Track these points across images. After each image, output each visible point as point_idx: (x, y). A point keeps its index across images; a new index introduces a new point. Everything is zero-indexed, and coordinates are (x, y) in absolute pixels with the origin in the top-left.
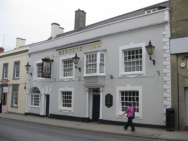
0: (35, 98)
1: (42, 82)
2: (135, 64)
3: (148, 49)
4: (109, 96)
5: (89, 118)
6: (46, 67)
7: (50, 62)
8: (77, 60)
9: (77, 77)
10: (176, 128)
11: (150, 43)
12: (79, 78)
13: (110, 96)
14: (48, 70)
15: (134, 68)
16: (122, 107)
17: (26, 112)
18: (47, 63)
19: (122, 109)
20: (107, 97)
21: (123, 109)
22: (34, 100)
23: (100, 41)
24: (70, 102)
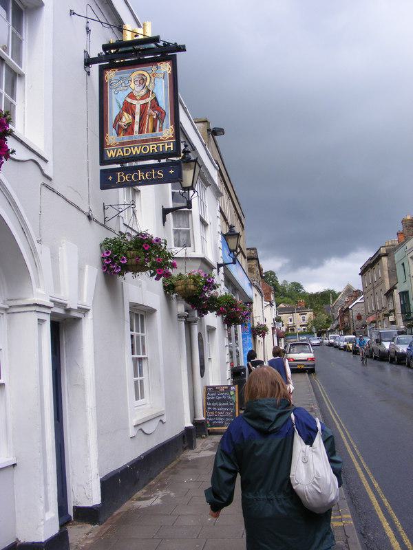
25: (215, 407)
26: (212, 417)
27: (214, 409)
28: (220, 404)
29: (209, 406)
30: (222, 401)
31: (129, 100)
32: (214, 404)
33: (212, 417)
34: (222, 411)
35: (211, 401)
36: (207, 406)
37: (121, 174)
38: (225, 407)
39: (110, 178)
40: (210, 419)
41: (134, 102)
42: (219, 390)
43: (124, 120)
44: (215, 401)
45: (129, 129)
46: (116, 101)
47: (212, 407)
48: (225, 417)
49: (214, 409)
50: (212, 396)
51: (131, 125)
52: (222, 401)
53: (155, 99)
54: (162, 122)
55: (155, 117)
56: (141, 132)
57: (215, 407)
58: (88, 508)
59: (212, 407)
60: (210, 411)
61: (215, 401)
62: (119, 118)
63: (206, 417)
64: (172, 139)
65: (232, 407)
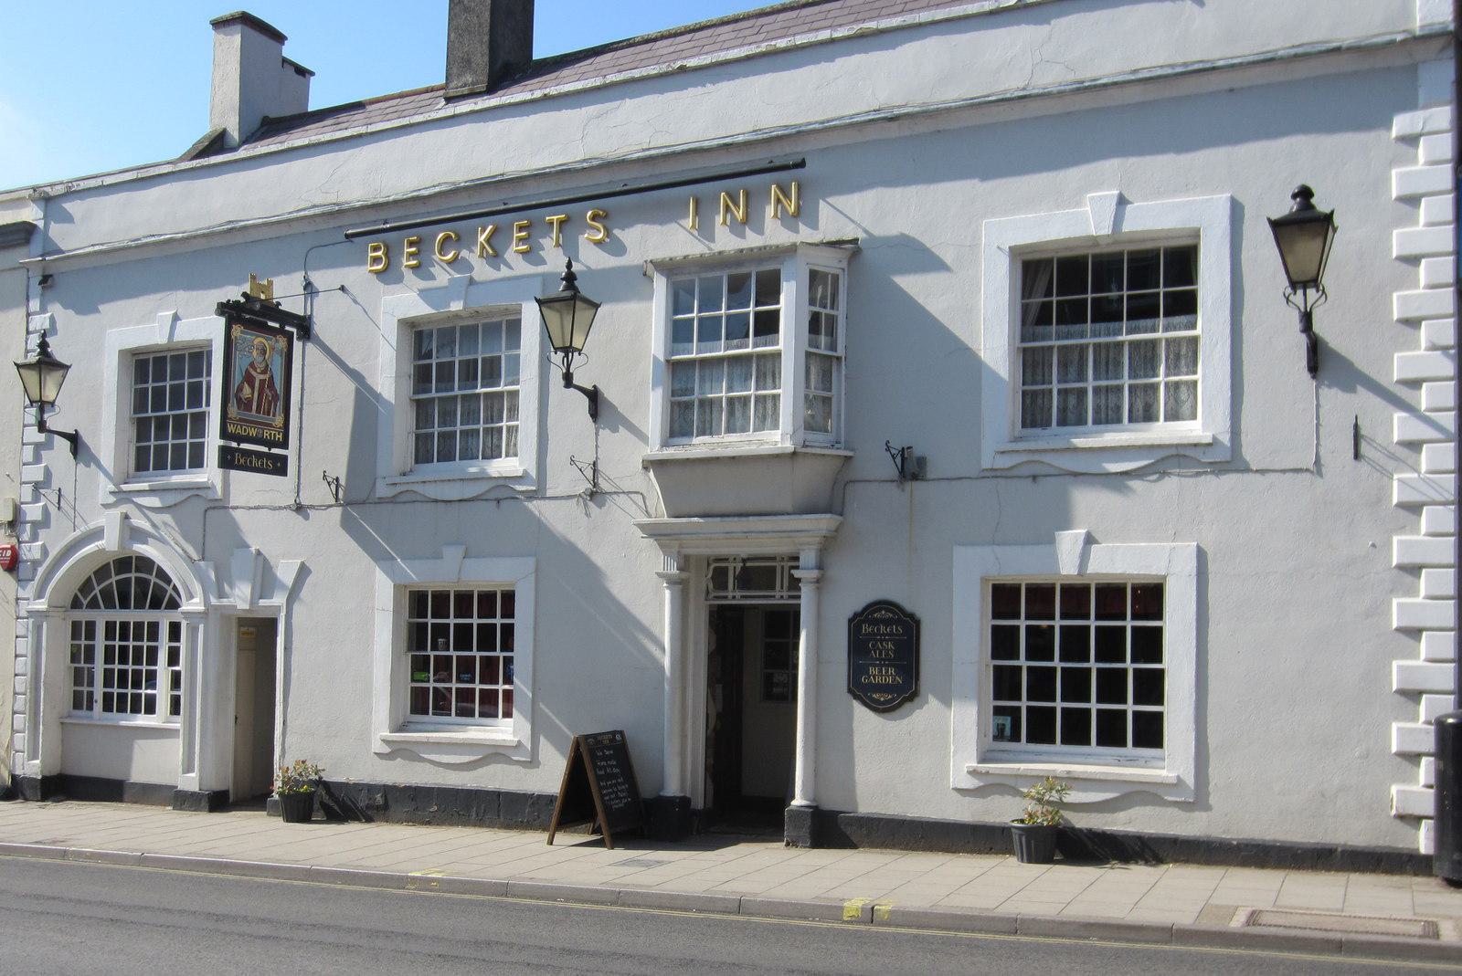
0: (91, 683)
1: (199, 506)
2: (1119, 364)
3: (553, 317)
4: (887, 622)
5: (684, 802)
6: (249, 379)
7: (281, 331)
8: (51, 381)
9: (572, 461)
10: (708, 431)
11: (1305, 194)
12: (589, 473)
13: (898, 622)
14: (264, 405)
15: (1072, 401)
16: (998, 711)
17: (102, 709)
18: (259, 340)
19: (1001, 720)
20: (866, 629)
21: (1007, 721)
22: (99, 666)
23: (802, 164)
24: (508, 644)
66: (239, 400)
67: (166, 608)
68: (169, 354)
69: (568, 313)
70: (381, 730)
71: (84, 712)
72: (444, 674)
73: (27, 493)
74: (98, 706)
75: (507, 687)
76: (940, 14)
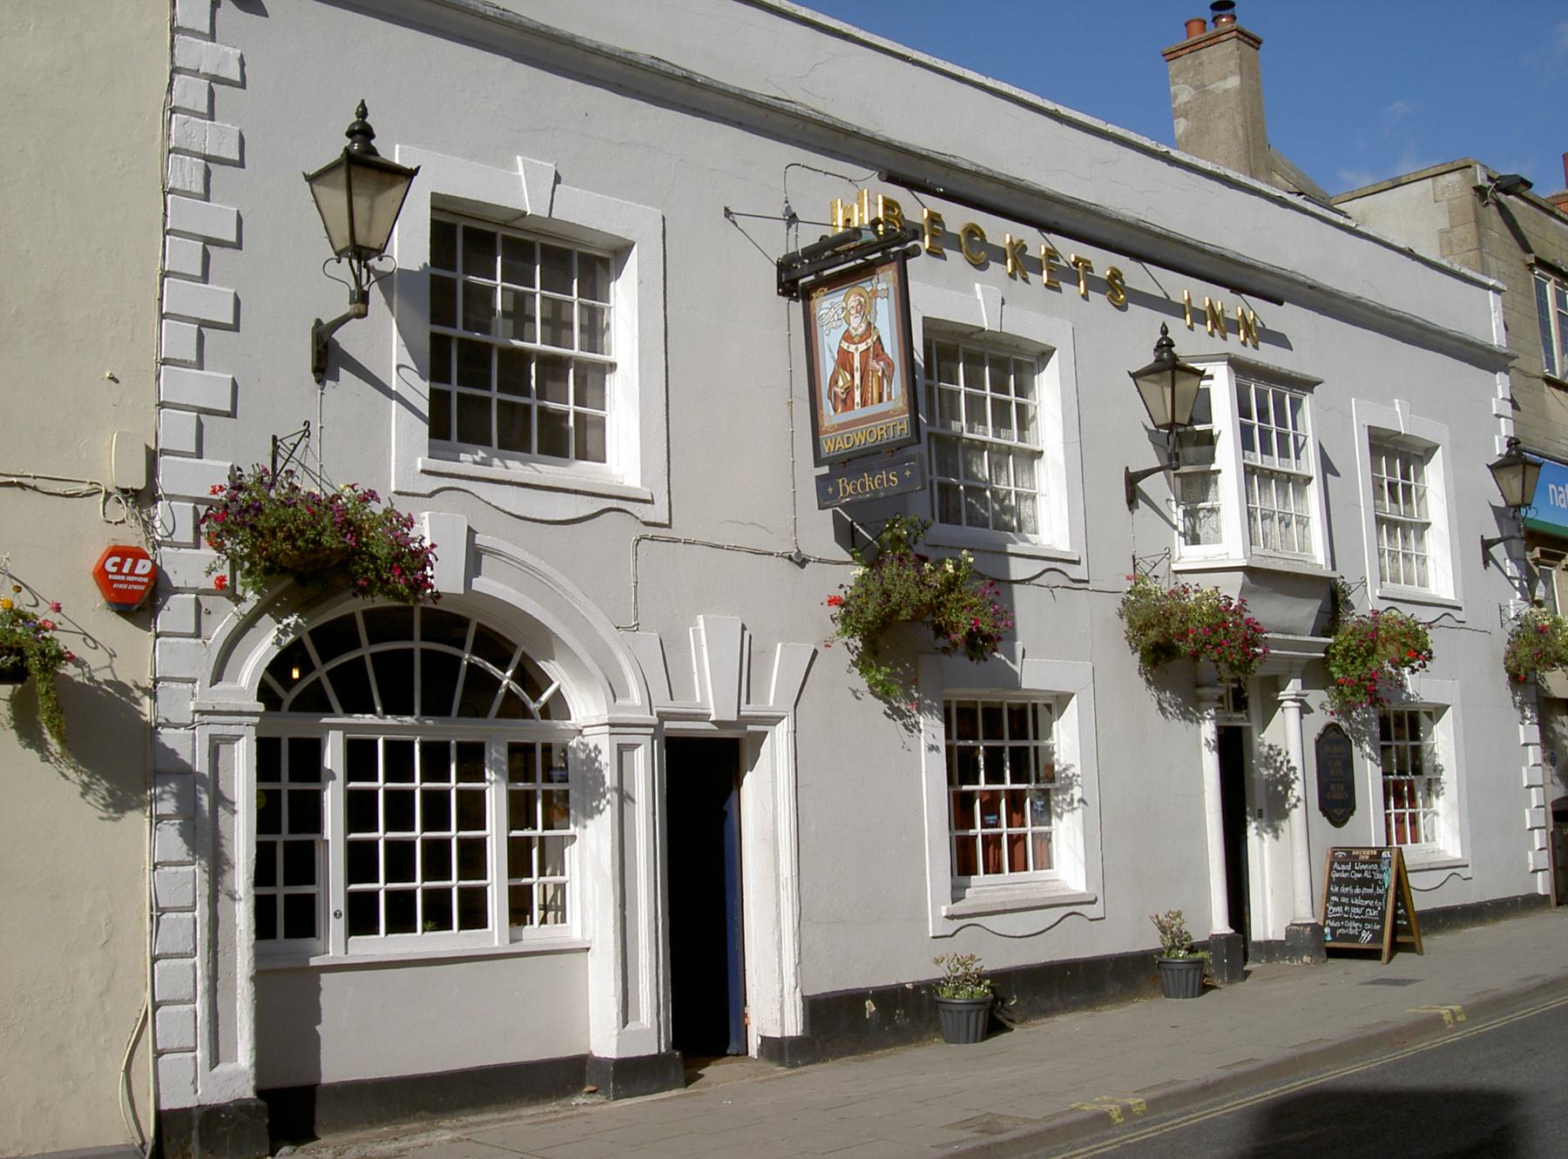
25: (1345, 895)
26: (1336, 919)
27: (1344, 900)
28: (1358, 891)
29: (1334, 895)
30: (1363, 883)
31: (845, 345)
32: (1345, 890)
33: (1336, 919)
34: (1360, 906)
35: (1339, 882)
36: (1329, 894)
37: (843, 481)
38: (1366, 897)
39: (830, 490)
40: (1332, 924)
41: (852, 348)
42: (1357, 856)
43: (841, 383)
44: (1348, 882)
45: (847, 403)
46: (830, 343)
47: (1339, 895)
48: (1362, 921)
49: (1344, 900)
50: (1343, 872)
51: (849, 391)
52: (1363, 883)
53: (879, 338)
54: (890, 382)
55: (880, 374)
56: (864, 404)
57: (1345, 895)
58: (257, 746)
59: (1339, 895)
60: (1336, 904)
61: (1348, 882)
62: (834, 381)
63: (1326, 918)
64: (903, 413)
65: (1380, 897)
66: (834, 397)
67: (499, 715)
68: (462, 223)
69: (1515, 476)
70: (937, 905)
71: (559, 925)
72: (991, 819)
73: (177, 430)
74: (336, 927)
75: (1411, 810)
76: (1121, 132)
